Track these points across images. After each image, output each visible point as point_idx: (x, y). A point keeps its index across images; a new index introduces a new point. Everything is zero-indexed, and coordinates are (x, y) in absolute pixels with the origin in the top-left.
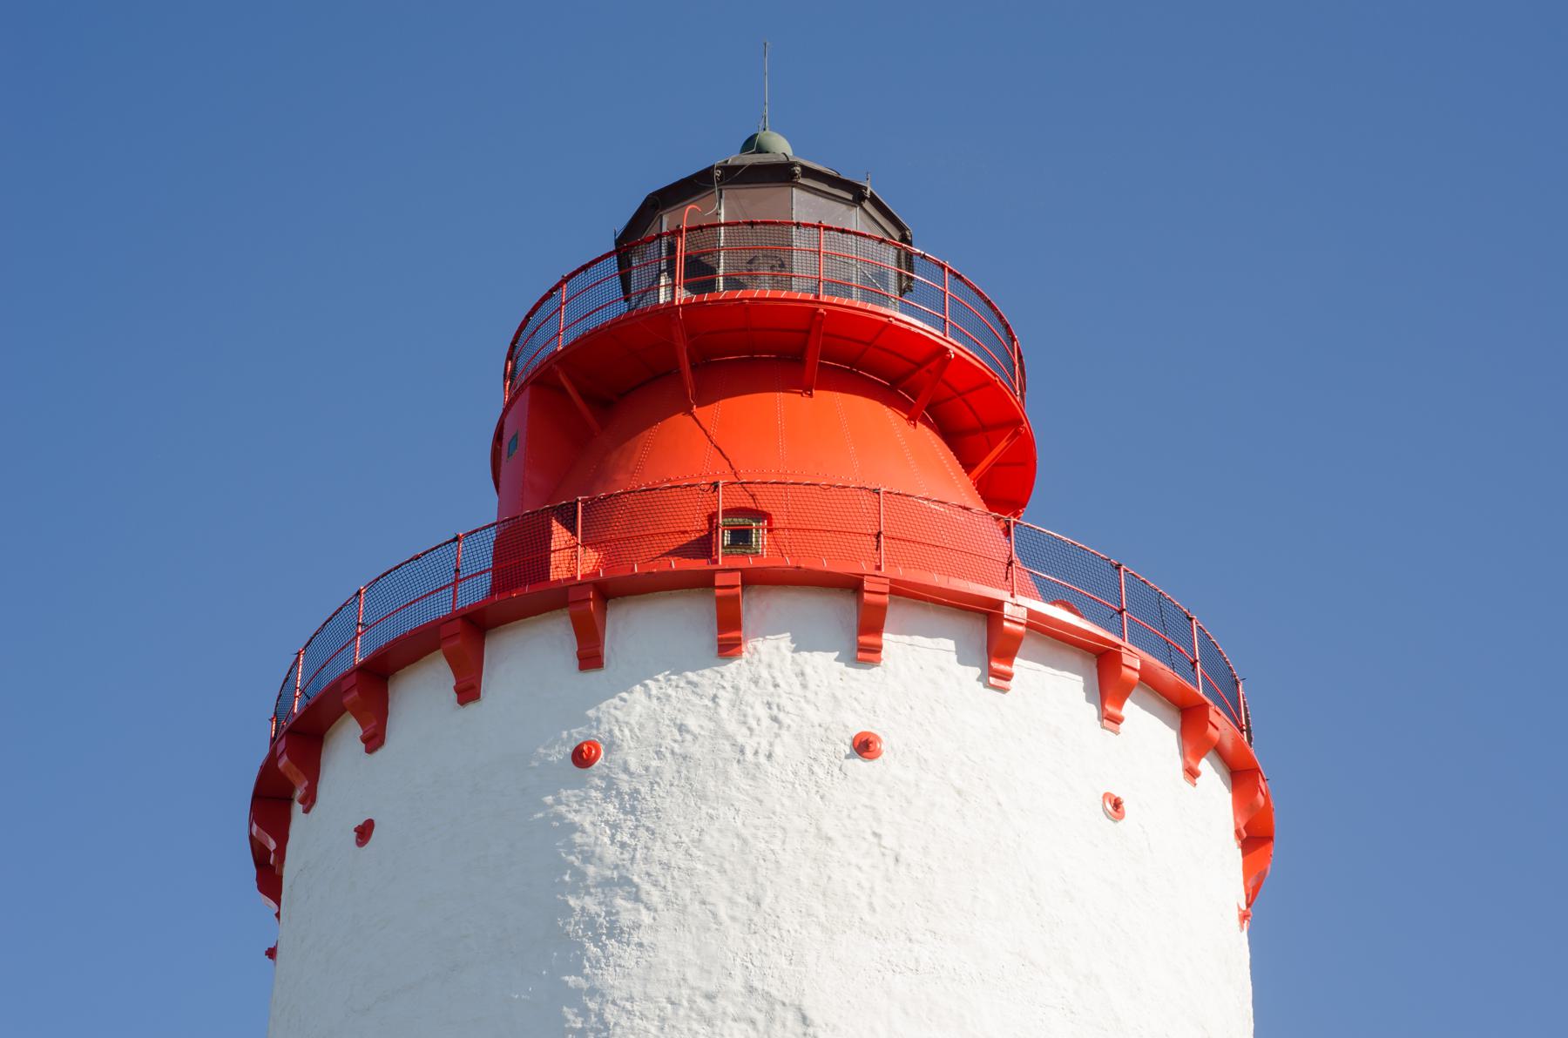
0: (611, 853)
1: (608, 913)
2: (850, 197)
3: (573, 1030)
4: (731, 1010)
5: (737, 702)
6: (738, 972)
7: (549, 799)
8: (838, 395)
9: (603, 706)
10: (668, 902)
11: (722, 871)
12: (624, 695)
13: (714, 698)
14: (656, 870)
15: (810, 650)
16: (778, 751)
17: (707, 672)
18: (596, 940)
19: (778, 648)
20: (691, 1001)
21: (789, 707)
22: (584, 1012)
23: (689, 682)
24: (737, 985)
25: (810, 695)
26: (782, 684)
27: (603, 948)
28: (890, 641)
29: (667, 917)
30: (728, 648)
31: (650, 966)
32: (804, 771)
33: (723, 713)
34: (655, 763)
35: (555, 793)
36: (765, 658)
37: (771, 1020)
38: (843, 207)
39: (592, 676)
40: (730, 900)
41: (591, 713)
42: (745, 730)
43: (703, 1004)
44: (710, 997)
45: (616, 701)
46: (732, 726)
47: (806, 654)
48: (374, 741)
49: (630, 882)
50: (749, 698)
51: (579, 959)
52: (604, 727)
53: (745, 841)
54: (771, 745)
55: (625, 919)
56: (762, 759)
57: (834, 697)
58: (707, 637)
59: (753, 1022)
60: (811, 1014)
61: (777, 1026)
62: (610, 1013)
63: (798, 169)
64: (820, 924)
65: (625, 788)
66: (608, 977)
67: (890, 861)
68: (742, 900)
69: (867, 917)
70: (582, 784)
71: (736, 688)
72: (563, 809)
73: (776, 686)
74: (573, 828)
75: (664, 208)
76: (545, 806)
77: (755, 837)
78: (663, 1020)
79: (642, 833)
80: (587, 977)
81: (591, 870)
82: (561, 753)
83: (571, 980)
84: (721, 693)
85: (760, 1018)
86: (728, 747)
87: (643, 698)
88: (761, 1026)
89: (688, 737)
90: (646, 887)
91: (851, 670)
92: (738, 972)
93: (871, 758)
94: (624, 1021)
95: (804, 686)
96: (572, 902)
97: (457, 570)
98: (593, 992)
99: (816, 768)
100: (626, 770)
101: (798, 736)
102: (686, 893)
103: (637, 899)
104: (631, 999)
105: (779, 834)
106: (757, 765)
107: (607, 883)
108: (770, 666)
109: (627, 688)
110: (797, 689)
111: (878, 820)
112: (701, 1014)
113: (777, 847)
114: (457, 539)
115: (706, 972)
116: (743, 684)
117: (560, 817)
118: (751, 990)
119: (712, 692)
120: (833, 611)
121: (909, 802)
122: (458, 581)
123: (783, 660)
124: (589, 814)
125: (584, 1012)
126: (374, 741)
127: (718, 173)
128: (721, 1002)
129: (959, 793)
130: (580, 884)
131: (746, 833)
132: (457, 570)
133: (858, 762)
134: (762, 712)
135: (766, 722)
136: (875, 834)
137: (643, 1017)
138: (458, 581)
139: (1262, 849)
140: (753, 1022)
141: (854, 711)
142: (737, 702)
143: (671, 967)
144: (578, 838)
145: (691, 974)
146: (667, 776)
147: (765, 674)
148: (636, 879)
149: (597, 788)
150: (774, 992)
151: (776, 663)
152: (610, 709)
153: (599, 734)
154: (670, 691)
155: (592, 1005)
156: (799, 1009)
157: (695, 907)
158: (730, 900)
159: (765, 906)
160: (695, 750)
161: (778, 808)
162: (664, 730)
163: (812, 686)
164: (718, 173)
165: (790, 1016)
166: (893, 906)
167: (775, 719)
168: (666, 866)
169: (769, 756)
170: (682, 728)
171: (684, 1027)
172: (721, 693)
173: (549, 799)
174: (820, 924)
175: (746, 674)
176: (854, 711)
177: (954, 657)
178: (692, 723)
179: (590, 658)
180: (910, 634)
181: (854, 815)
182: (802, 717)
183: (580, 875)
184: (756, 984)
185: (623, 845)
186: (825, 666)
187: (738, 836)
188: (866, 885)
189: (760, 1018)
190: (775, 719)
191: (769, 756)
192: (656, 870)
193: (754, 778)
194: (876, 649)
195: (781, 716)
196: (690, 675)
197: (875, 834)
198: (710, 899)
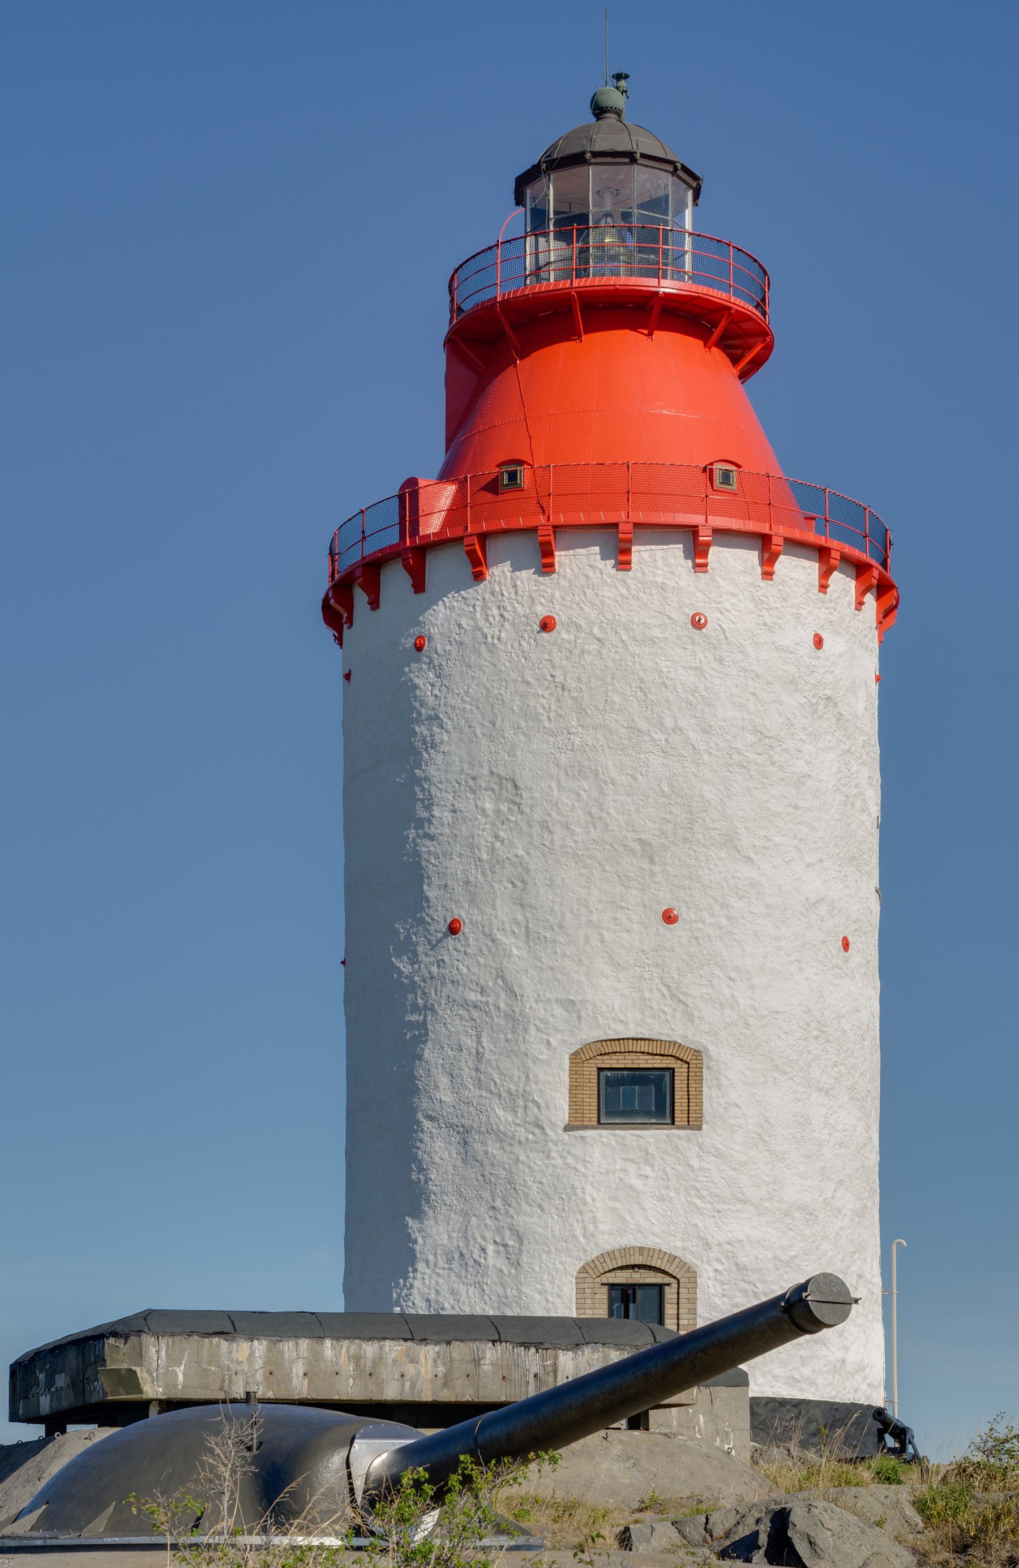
0: (431, 701)
1: (431, 735)
2: (628, 160)
3: (419, 799)
4: (483, 784)
5: (485, 608)
6: (485, 764)
7: (407, 669)
8: (597, 334)
9: (426, 614)
10: (455, 728)
11: (478, 708)
12: (435, 607)
13: (474, 606)
14: (449, 710)
15: (519, 570)
16: (503, 635)
17: (470, 591)
18: (426, 750)
19: (503, 572)
20: (466, 781)
21: (509, 608)
22: (423, 790)
23: (463, 598)
24: (486, 772)
25: (519, 599)
26: (505, 593)
27: (429, 754)
28: (560, 557)
29: (455, 736)
30: (479, 577)
31: (448, 764)
32: (516, 645)
33: (478, 615)
34: (448, 648)
35: (409, 666)
36: (497, 579)
37: (501, 788)
38: (625, 168)
39: (421, 596)
40: (482, 725)
41: (421, 618)
42: (488, 625)
43: (471, 783)
44: (474, 779)
45: (431, 611)
46: (482, 623)
47: (518, 573)
48: (375, 604)
49: (438, 718)
50: (490, 605)
51: (420, 760)
52: (427, 627)
53: (488, 690)
54: (500, 631)
55: (437, 739)
56: (496, 641)
57: (531, 597)
58: (468, 569)
59: (493, 790)
60: (520, 784)
61: (504, 792)
62: (433, 790)
63: (588, 155)
64: (523, 732)
65: (436, 663)
66: (432, 771)
67: (560, 690)
68: (487, 724)
69: (547, 724)
70: (418, 661)
71: (484, 599)
72: (412, 675)
73: (503, 595)
74: (416, 687)
75: (526, 185)
76: (405, 674)
77: (492, 686)
78: (455, 792)
79: (444, 689)
80: (423, 770)
81: (423, 711)
82: (409, 643)
83: (417, 771)
84: (478, 603)
85: (496, 787)
86: (480, 636)
87: (443, 609)
88: (497, 792)
89: (462, 631)
90: (445, 720)
91: (541, 579)
92: (485, 764)
93: (550, 631)
94: (439, 795)
95: (516, 593)
96: (417, 729)
97: (363, 532)
98: (426, 779)
99: (522, 642)
100: (436, 652)
101: (513, 625)
102: (463, 722)
103: (442, 727)
104: (441, 782)
105: (504, 684)
106: (493, 644)
107: (430, 718)
108: (500, 583)
109: (436, 603)
110: (513, 595)
111: (553, 667)
112: (470, 788)
113: (503, 692)
114: (362, 511)
115: (472, 765)
116: (487, 596)
117: (411, 680)
118: (492, 773)
119: (473, 602)
120: (526, 546)
121: (571, 652)
122: (364, 538)
123: (506, 579)
124: (423, 679)
125: (423, 790)
126: (375, 604)
127: (544, 166)
128: (479, 781)
129: (599, 640)
130: (419, 721)
131: (488, 685)
132: (363, 532)
133: (544, 635)
134: (495, 611)
135: (498, 618)
136: (552, 676)
137: (446, 791)
138: (364, 538)
139: (868, 574)
140: (493, 790)
141: (541, 604)
142: (485, 608)
143: (457, 764)
144: (418, 693)
145: (465, 766)
146: (454, 655)
147: (497, 589)
148: (441, 716)
149: (425, 663)
150: (502, 773)
151: (503, 581)
152: (428, 616)
153: (424, 631)
154: (455, 604)
155: (426, 786)
156: (513, 781)
157: (467, 729)
158: (482, 725)
159: (497, 726)
160: (466, 639)
161: (503, 669)
162: (452, 627)
163: (520, 593)
164: (544, 166)
165: (510, 785)
166: (561, 716)
167: (502, 616)
168: (453, 708)
169: (499, 639)
170: (460, 626)
171: (463, 795)
172: (478, 603)
173: (407, 669)
174: (523, 732)
175: (489, 590)
176: (541, 604)
177: (598, 557)
178: (464, 622)
179: (419, 586)
180: (573, 549)
181: (541, 666)
182: (515, 612)
183: (419, 713)
184: (494, 770)
185: (436, 696)
186: (527, 576)
187: (485, 687)
188: (546, 705)
189: (496, 787)
190: (502, 616)
191: (499, 639)
192: (449, 710)
193: (492, 652)
194: (552, 565)
195: (505, 613)
196: (463, 592)
197: (552, 676)
198: (473, 725)
